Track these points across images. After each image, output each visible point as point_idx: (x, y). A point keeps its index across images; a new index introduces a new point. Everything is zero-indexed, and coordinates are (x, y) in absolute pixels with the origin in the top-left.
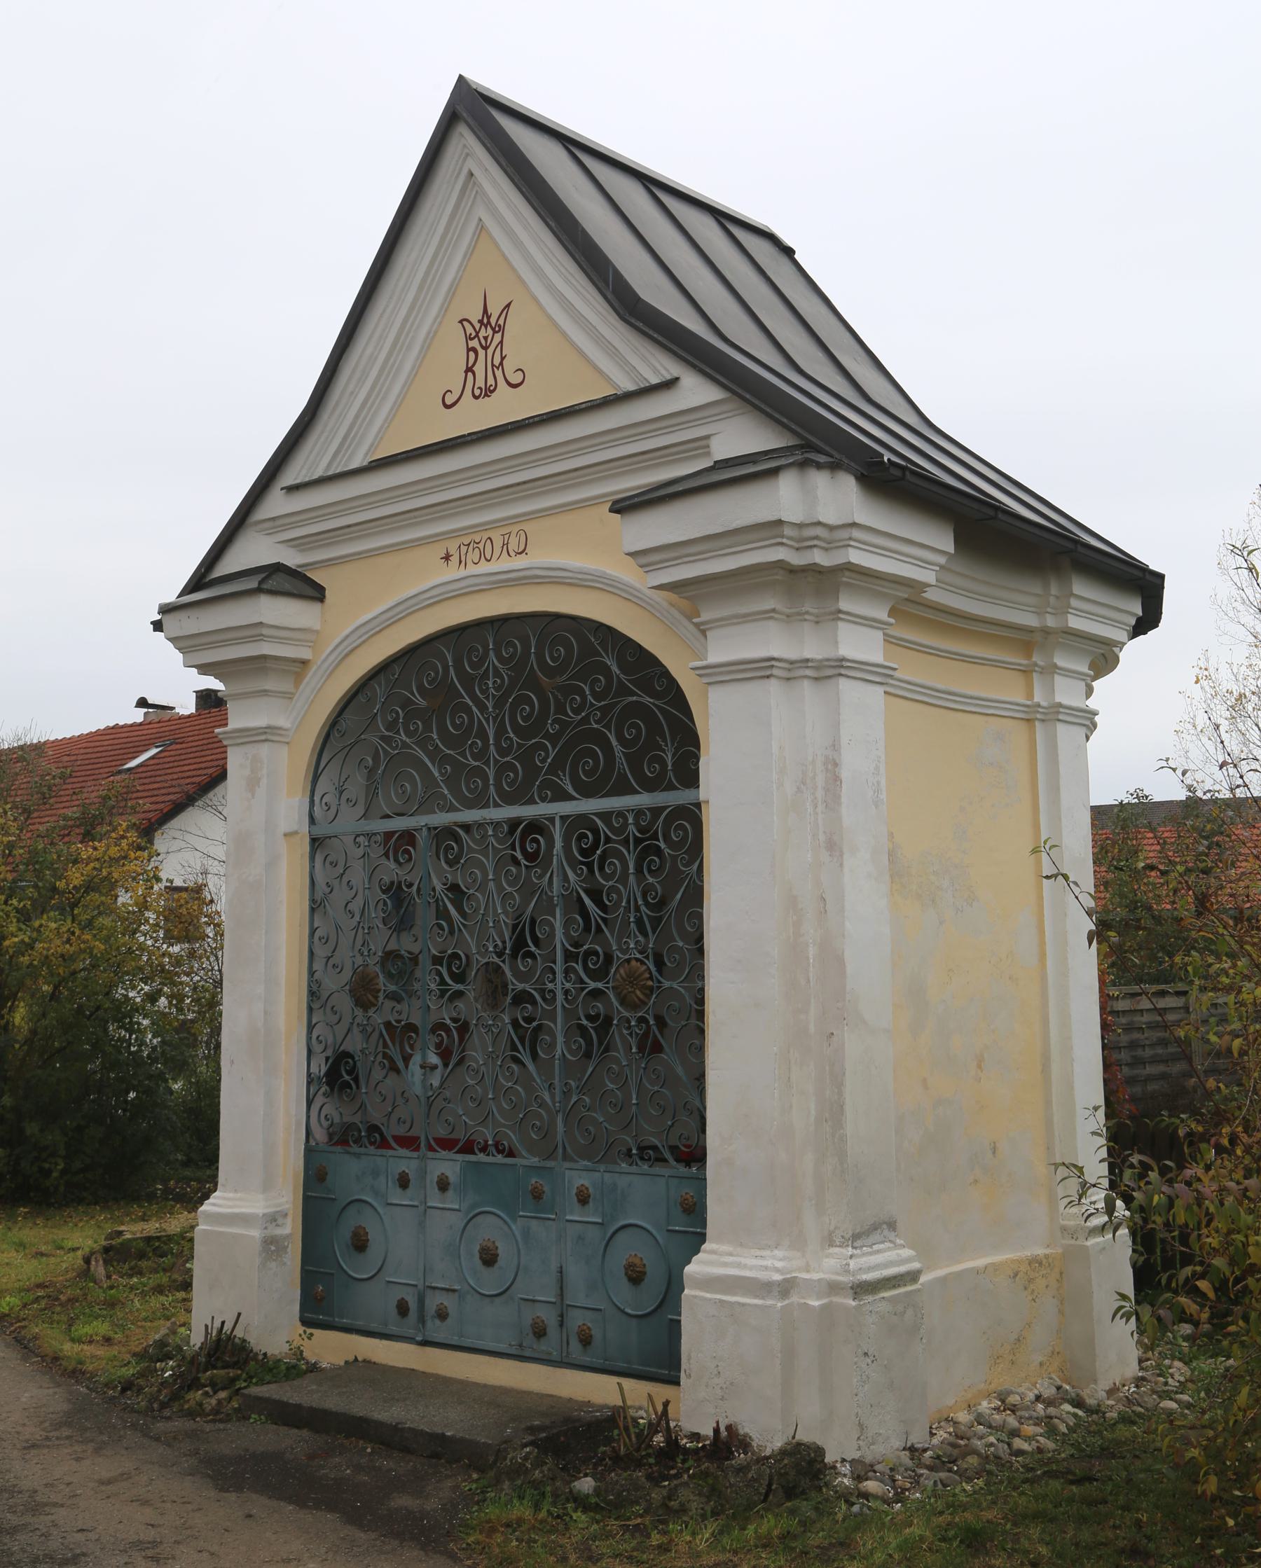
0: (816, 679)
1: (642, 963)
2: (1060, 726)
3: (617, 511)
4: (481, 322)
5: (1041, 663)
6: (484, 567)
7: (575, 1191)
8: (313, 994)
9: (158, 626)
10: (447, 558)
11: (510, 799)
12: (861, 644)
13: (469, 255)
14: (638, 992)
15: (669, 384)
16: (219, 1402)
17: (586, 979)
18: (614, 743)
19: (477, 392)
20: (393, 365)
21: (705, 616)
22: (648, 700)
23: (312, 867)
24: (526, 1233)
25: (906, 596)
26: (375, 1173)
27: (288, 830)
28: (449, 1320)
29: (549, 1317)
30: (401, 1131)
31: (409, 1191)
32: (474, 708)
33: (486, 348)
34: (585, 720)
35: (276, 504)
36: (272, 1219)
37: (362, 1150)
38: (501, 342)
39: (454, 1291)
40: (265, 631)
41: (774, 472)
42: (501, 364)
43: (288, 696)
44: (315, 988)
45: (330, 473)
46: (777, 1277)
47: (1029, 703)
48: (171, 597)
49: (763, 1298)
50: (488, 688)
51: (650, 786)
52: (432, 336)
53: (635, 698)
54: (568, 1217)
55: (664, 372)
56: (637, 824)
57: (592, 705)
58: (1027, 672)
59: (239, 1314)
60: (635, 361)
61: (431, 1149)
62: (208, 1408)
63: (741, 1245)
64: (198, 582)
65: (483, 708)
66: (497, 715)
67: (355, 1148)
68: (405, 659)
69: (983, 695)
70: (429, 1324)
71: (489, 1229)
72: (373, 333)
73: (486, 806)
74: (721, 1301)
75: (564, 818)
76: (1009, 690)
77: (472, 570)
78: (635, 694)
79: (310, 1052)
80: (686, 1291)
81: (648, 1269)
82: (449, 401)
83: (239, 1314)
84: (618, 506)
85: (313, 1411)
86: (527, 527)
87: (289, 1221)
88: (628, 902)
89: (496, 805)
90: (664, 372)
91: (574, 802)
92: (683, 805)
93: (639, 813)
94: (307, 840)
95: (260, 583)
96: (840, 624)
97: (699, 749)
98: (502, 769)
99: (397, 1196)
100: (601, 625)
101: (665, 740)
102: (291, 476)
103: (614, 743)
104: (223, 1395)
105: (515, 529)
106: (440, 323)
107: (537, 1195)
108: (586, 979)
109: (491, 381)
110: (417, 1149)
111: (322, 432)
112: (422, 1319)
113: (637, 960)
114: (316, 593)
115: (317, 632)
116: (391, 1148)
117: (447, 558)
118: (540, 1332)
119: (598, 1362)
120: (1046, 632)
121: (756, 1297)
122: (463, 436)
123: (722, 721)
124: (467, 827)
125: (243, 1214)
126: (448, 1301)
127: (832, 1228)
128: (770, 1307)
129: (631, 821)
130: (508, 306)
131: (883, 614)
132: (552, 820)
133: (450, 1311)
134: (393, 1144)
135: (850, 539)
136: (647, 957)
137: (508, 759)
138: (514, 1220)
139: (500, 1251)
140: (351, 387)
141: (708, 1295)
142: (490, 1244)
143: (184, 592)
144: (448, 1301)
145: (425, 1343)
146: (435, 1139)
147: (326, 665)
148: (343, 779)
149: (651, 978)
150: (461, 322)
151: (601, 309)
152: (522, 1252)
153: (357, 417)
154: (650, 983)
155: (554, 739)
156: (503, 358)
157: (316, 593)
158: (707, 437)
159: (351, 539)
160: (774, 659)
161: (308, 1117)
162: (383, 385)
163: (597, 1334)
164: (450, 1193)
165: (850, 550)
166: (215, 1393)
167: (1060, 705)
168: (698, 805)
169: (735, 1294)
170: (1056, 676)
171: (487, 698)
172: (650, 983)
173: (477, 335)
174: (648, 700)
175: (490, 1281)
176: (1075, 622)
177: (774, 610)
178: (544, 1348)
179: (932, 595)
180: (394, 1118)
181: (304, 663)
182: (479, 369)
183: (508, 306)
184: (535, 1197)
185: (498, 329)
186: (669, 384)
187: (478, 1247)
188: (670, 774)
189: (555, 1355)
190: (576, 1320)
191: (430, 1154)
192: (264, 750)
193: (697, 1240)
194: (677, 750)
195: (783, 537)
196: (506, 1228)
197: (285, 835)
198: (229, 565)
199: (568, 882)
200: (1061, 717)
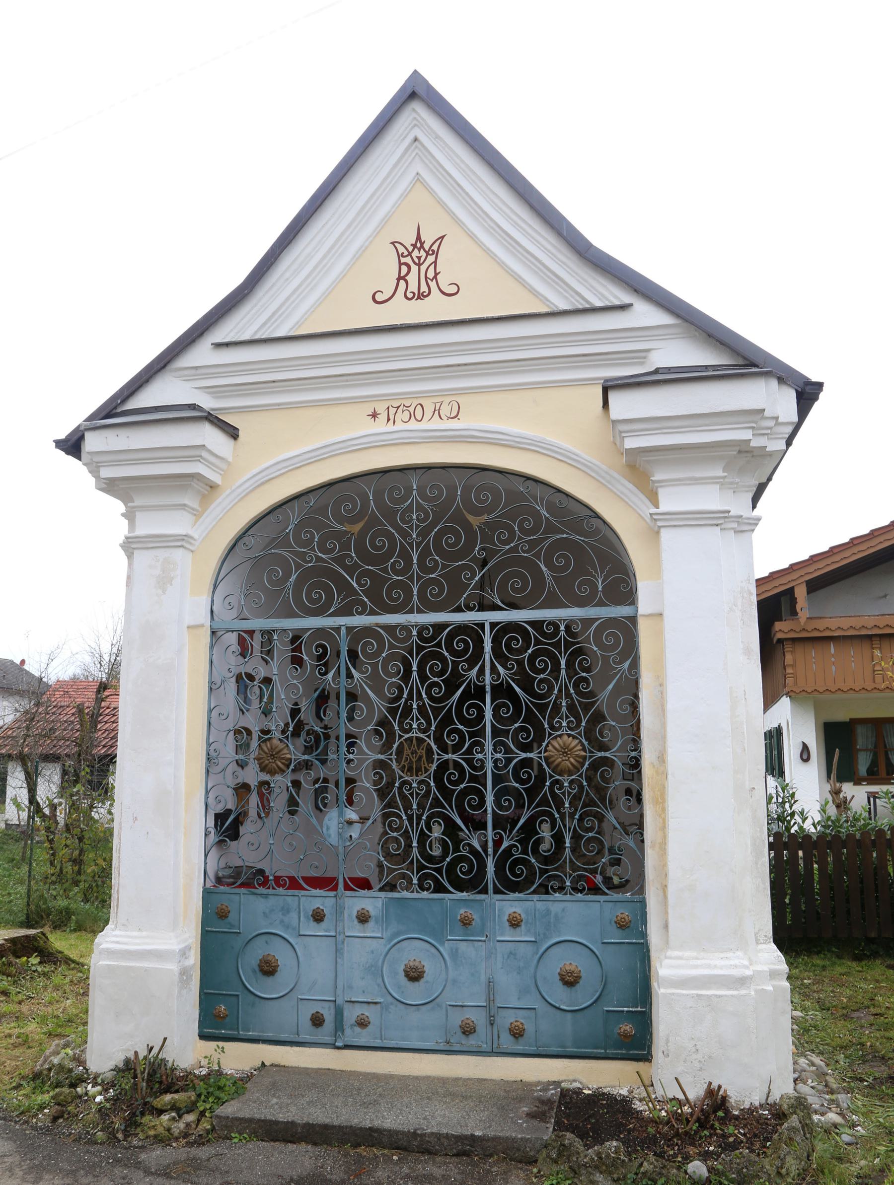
1: (574, 737)
4: (414, 246)
6: (413, 425)
7: (506, 917)
13: (405, 195)
14: (572, 760)
16: (188, 1125)
18: (544, 569)
19: (410, 295)
20: (324, 266)
23: (211, 655)
24: (454, 954)
26: (286, 910)
27: (192, 623)
28: (370, 1028)
29: (478, 1018)
31: (323, 925)
33: (419, 265)
34: (515, 549)
35: (202, 354)
36: (183, 953)
37: (271, 891)
39: (376, 1003)
40: (204, 454)
42: (435, 277)
45: (257, 337)
49: (737, 989)
50: (412, 519)
53: (565, 536)
54: (499, 938)
59: (165, 1039)
61: (347, 888)
62: (176, 1132)
63: (704, 950)
67: (262, 890)
68: (476, 471)
70: (348, 1031)
71: (414, 952)
72: (315, 237)
73: (411, 612)
74: (698, 995)
75: (493, 625)
77: (399, 426)
81: (583, 974)
82: (379, 298)
83: (165, 1039)
85: (309, 1126)
86: (460, 399)
87: (192, 952)
88: (560, 690)
89: (420, 611)
92: (615, 618)
94: (209, 633)
99: (312, 928)
101: (596, 572)
102: (224, 332)
103: (544, 569)
104: (190, 1118)
105: (447, 400)
106: (371, 242)
107: (466, 922)
109: (424, 288)
110: (335, 888)
111: (255, 305)
113: (569, 735)
115: (229, 463)
116: (302, 888)
117: (374, 415)
118: (468, 1030)
119: (533, 1049)
121: (730, 989)
125: (156, 951)
126: (367, 1011)
127: (756, 930)
128: (745, 995)
130: (442, 237)
132: (482, 626)
133: (371, 1019)
138: (442, 944)
139: (426, 969)
140: (287, 275)
141: (684, 992)
142: (417, 964)
146: (349, 878)
147: (240, 490)
150: (393, 243)
152: (450, 968)
153: (288, 299)
156: (436, 274)
163: (529, 1028)
164: (371, 924)
166: (180, 1117)
169: (709, 989)
171: (411, 528)
175: (415, 993)
178: (473, 1042)
181: (213, 487)
182: (412, 278)
183: (442, 237)
184: (465, 924)
186: (623, 307)
187: (403, 967)
189: (485, 1047)
190: (507, 1019)
191: (348, 893)
192: (178, 555)
196: (433, 950)
198: (145, 399)
199: (499, 675)
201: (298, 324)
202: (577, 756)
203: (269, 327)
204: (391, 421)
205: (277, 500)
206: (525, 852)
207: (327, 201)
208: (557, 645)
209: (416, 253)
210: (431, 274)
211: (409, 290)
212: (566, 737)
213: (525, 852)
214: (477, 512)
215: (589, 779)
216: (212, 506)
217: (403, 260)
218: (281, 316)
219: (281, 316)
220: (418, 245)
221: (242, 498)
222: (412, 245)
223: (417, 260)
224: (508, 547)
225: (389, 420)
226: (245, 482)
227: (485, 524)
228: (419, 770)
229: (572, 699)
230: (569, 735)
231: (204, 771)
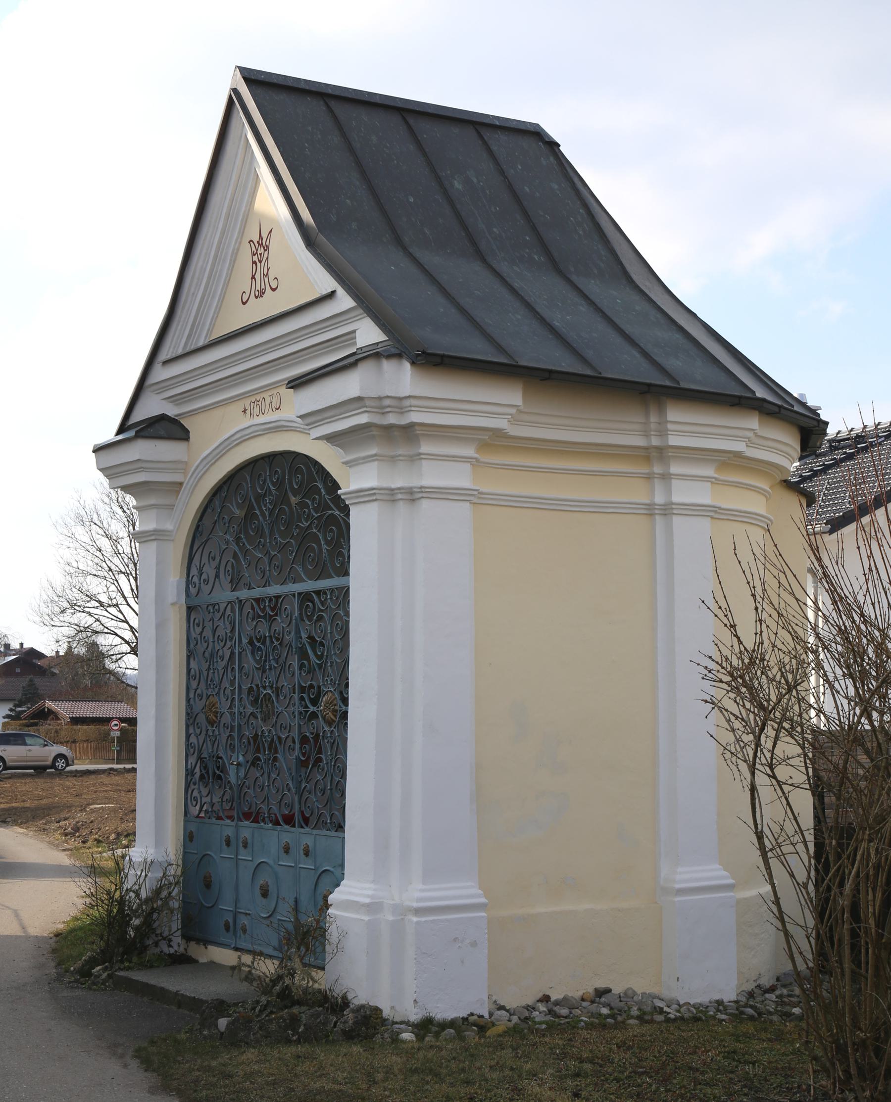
4: (258, 242)
10: (245, 411)
17: (309, 705)
19: (257, 293)
35: (160, 374)
43: (171, 507)
54: (281, 863)
58: (649, 477)
65: (264, 516)
76: (637, 493)
84: (293, 384)
96: (423, 461)
102: (163, 355)
106: (240, 243)
108: (309, 705)
109: (263, 287)
111: (179, 322)
115: (186, 463)
117: (245, 411)
123: (365, 527)
124: (318, 593)
130: (271, 231)
135: (411, 406)
143: (118, 434)
158: (354, 332)
159: (190, 400)
160: (374, 489)
165: (412, 413)
170: (673, 481)
176: (673, 441)
177: (375, 455)
183: (271, 231)
185: (266, 248)
186: (332, 295)
197: (172, 604)
198: (136, 417)
200: (675, 512)
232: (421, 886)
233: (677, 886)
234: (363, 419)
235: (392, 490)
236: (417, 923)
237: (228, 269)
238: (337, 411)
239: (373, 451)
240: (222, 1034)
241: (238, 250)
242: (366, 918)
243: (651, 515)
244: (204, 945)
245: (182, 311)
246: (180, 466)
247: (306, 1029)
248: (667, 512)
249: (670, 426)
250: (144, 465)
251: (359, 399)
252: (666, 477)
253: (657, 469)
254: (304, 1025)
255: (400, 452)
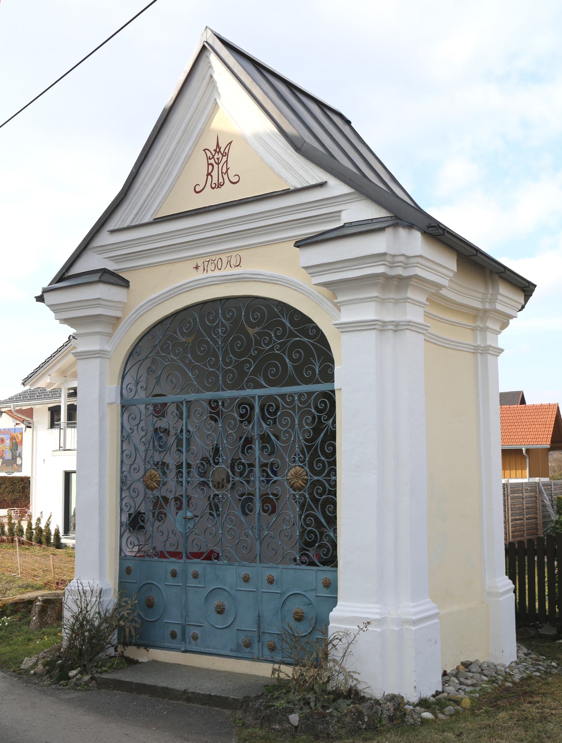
0: (382, 330)
1: (302, 467)
2: (489, 356)
3: (298, 247)
4: (215, 150)
5: (481, 326)
6: (217, 273)
8: (123, 482)
9: (40, 299)
10: (197, 268)
11: (231, 388)
12: (414, 314)
14: (300, 482)
15: (322, 185)
18: (287, 360)
19: (213, 186)
21: (339, 299)
22: (305, 340)
25: (434, 291)
30: (172, 549)
31: (176, 578)
32: (211, 342)
33: (218, 164)
34: (272, 349)
35: (105, 238)
38: (227, 161)
41: (382, 229)
42: (227, 172)
44: (124, 480)
46: (378, 617)
47: (476, 345)
48: (46, 285)
50: (218, 332)
51: (307, 382)
52: (188, 157)
53: (298, 339)
55: (318, 178)
56: (299, 400)
57: (275, 342)
58: (474, 329)
60: (301, 172)
61: (188, 558)
64: (62, 277)
65: (216, 342)
66: (224, 346)
68: (174, 316)
69: (464, 342)
73: (218, 390)
76: (465, 337)
77: (210, 274)
78: (298, 336)
79: (121, 510)
80: (331, 625)
82: (197, 190)
86: (242, 253)
88: (295, 438)
89: (223, 390)
90: (318, 178)
91: (263, 390)
93: (301, 395)
95: (100, 278)
96: (407, 304)
97: (334, 364)
98: (225, 373)
99: (171, 581)
100: (280, 302)
101: (315, 362)
102: (113, 224)
103: (287, 360)
105: (234, 254)
106: (193, 151)
108: (272, 476)
109: (221, 180)
110: (181, 558)
111: (130, 204)
112: (184, 639)
113: (300, 466)
114: (125, 284)
115: (125, 303)
116: (166, 557)
117: (197, 268)
120: (485, 311)
122: (206, 207)
123: (341, 348)
129: (296, 399)
130: (230, 143)
131: (423, 299)
132: (254, 397)
134: (167, 556)
135: (417, 263)
136: (305, 465)
137: (230, 367)
140: (145, 181)
144: (197, 631)
145: (186, 651)
148: (139, 377)
149: (307, 475)
150: (204, 150)
151: (283, 146)
154: (306, 477)
155: (254, 358)
156: (227, 169)
157: (125, 284)
158: (340, 211)
161: (121, 543)
162: (162, 180)
165: (417, 268)
167: (490, 346)
168: (333, 392)
170: (488, 332)
172: (306, 477)
173: (213, 157)
174: (305, 340)
176: (499, 307)
177: (377, 297)
179: (444, 292)
180: (168, 544)
181: (118, 319)
182: (215, 174)
183: (230, 143)
185: (225, 154)
186: (322, 185)
188: (317, 376)
191: (189, 561)
193: (333, 601)
194: (321, 364)
195: (385, 261)
197: (108, 404)
198: (78, 269)
200: (490, 352)
201: (156, 211)
202: (303, 479)
203: (140, 215)
204: (206, 271)
205: (122, 360)
206: (319, 417)
207: (163, 129)
208: (293, 409)
209: (216, 156)
210: (224, 171)
211: (213, 183)
212: (298, 468)
213: (319, 417)
214: (253, 326)
215: (311, 494)
216: (120, 327)
217: (210, 161)
218: (146, 207)
219: (146, 207)
220: (218, 150)
221: (132, 324)
222: (214, 150)
223: (217, 161)
224: (268, 347)
225: (204, 270)
226: (134, 313)
227: (257, 333)
228: (223, 487)
229: (301, 443)
230: (300, 466)
231: (119, 488)
232: (412, 604)
233: (501, 591)
234: (380, 270)
235: (385, 322)
236: (416, 630)
237: (181, 168)
238: (356, 263)
239: (375, 294)
240: (296, 727)
241: (191, 155)
242: (379, 630)
243: (474, 353)
244: (146, 648)
245: (134, 196)
246: (123, 306)
247: (369, 717)
248: (484, 352)
249: (499, 297)
250: (101, 302)
251: (385, 254)
252: (484, 330)
253: (479, 323)
254: (367, 715)
255: (392, 296)
